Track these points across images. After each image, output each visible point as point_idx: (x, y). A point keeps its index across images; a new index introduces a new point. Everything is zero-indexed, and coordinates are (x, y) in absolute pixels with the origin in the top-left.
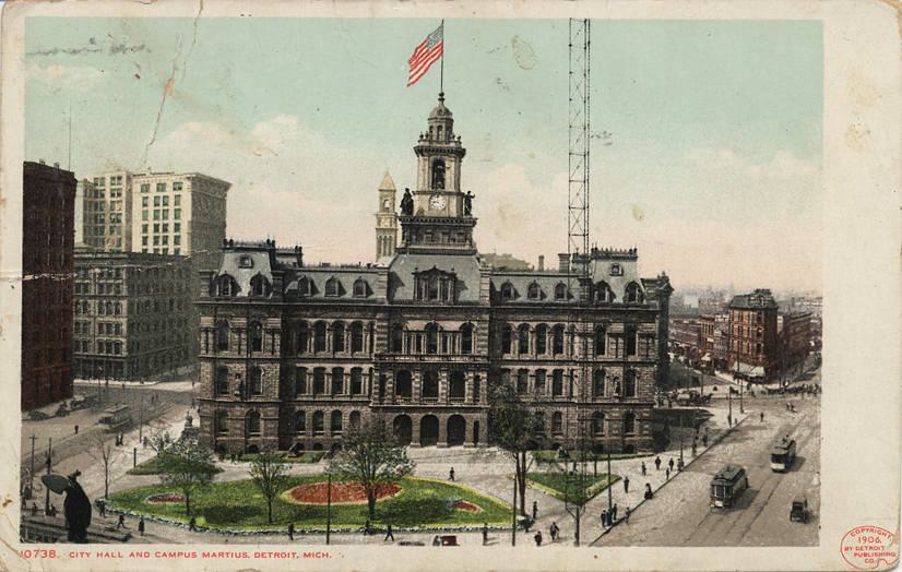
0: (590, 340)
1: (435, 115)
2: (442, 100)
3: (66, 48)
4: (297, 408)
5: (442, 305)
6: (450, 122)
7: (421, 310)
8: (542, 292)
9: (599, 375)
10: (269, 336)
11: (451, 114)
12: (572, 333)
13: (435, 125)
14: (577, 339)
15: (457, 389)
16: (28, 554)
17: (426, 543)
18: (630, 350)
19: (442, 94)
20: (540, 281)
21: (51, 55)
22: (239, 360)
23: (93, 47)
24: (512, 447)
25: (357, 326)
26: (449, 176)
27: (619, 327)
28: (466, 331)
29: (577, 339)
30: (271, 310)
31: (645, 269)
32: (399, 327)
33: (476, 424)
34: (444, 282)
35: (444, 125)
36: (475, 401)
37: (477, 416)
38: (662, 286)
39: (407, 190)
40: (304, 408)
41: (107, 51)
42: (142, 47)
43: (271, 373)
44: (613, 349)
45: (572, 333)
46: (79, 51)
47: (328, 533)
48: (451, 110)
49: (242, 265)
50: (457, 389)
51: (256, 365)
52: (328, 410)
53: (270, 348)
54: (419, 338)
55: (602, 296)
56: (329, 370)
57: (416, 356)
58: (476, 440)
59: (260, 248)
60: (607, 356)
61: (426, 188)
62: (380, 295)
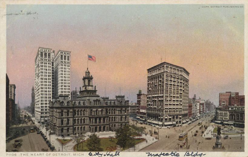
0: (60, 113)
2: (88, 69)
3: (14, 13)
5: (98, 106)
7: (96, 107)
9: (62, 121)
16: (65, 155)
17: (148, 143)
20: (76, 101)
21: (10, 15)
22: (65, 118)
23: (22, 13)
24: (220, 130)
28: (102, 111)
30: (71, 108)
31: (126, 99)
32: (91, 110)
33: (93, 128)
37: (93, 127)
38: (210, 102)
40: (76, 126)
41: (26, 14)
42: (35, 13)
43: (71, 120)
46: (18, 14)
52: (80, 126)
55: (62, 104)
56: (80, 119)
60: (64, 117)
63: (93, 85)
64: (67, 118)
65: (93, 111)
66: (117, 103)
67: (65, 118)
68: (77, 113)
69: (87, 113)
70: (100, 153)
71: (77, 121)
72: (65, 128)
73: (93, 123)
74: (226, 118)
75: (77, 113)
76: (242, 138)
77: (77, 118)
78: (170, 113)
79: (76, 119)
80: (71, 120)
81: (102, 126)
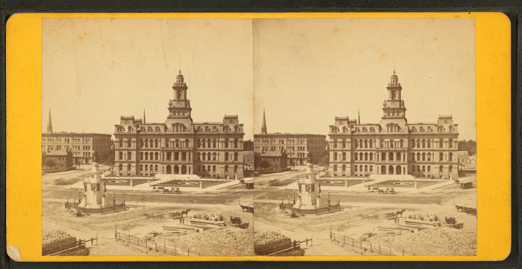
1: (178, 77)
4: (141, 164)
6: (182, 79)
8: (209, 129)
10: (125, 143)
11: (183, 76)
12: (218, 142)
13: (393, 80)
14: (220, 143)
15: (184, 158)
18: (236, 146)
19: (180, 71)
22: (340, 150)
25: (371, 141)
26: (183, 95)
27: (447, 140)
29: (220, 143)
34: (395, 126)
35: (395, 80)
36: (189, 161)
37: (189, 166)
39: (170, 100)
44: (445, 146)
45: (218, 142)
47: (329, 195)
48: (397, 75)
49: (126, 123)
50: (184, 158)
51: (442, 152)
53: (455, 147)
54: (388, 143)
57: (395, 148)
58: (190, 173)
59: (344, 120)
60: (338, 148)
61: (176, 99)
62: (377, 132)
63: (381, 119)
64: (235, 150)
65: (171, 142)
66: (221, 130)
67: (340, 150)
68: (359, 144)
69: (162, 144)
70: (217, 243)
71: (359, 157)
72: (445, 166)
73: (165, 160)
74: (86, 153)
75: (359, 144)
76: (84, 223)
77: (201, 153)
78: (292, 143)
79: (414, 153)
80: (348, 154)
81: (386, 166)
